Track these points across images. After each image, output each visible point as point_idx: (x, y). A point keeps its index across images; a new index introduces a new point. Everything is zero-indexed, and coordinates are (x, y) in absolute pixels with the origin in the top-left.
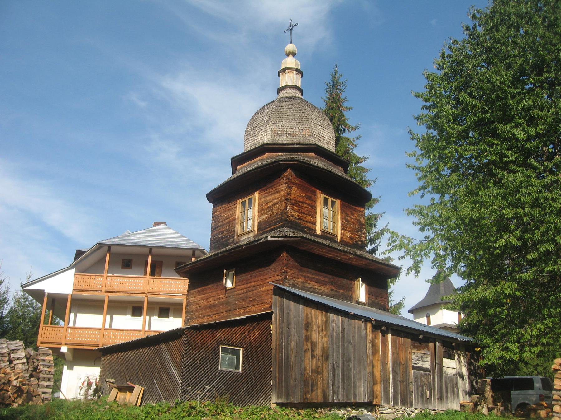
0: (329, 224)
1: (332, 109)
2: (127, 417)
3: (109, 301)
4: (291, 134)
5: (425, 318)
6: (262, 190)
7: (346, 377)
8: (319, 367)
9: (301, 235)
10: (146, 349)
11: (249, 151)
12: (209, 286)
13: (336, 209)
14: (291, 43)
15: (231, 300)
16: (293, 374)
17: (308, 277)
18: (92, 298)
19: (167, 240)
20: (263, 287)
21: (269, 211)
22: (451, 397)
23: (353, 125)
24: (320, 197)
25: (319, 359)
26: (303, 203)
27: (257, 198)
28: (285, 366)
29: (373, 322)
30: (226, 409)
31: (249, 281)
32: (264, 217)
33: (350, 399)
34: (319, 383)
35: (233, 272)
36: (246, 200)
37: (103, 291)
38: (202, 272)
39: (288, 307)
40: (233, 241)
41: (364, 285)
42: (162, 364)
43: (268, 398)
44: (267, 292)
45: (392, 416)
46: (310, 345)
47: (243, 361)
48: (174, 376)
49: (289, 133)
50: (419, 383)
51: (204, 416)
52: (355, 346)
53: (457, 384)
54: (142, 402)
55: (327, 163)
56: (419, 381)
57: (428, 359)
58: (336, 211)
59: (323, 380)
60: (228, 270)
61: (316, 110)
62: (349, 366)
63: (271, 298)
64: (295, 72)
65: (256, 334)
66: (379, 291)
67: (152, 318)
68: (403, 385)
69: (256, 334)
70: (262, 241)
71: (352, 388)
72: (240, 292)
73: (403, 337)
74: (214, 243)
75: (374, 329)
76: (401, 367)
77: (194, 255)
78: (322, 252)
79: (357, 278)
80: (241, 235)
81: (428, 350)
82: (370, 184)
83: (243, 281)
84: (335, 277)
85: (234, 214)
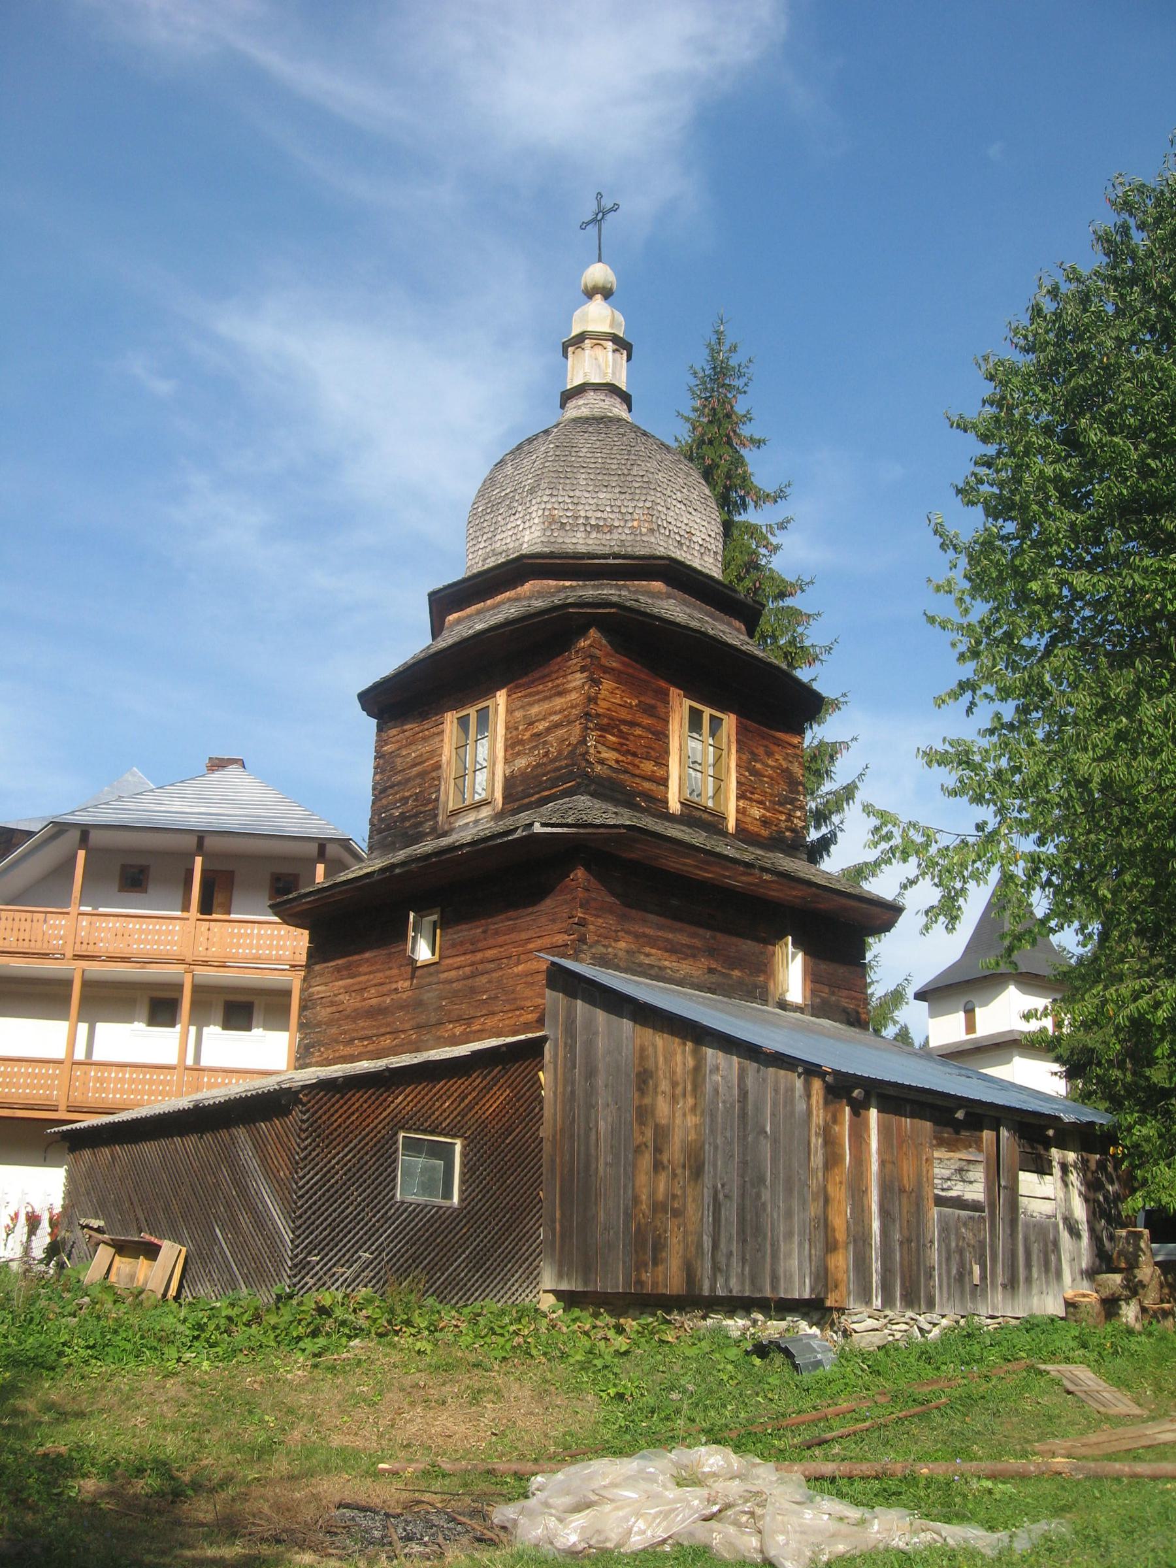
0: (705, 782)
1: (711, 442)
2: (142, 1337)
3: (87, 984)
4: (598, 526)
5: (961, 1016)
6: (517, 687)
7: (752, 1230)
8: (674, 1196)
9: (625, 817)
10: (194, 1138)
11: (480, 574)
12: (367, 955)
13: (725, 740)
14: (600, 260)
15: (428, 996)
16: (602, 1214)
17: (644, 935)
18: (35, 974)
19: (246, 812)
20: (518, 963)
21: (535, 747)
22: (1039, 1278)
23: (770, 489)
24: (680, 706)
25: (675, 1175)
26: (632, 724)
27: (502, 709)
28: (580, 1190)
29: (828, 1078)
30: (417, 1320)
31: (480, 945)
32: (521, 763)
33: (760, 1291)
34: (675, 1240)
35: (435, 917)
36: (472, 712)
37: (69, 954)
38: (349, 917)
39: (589, 1024)
40: (434, 829)
41: (800, 956)
42: (237, 1183)
43: (532, 1277)
44: (529, 979)
45: (877, 1339)
46: (649, 1133)
47: (462, 1174)
48: (272, 1219)
49: (593, 522)
50: (953, 1244)
51: (356, 1336)
52: (775, 1141)
53: (1056, 1244)
54: (181, 1286)
55: (700, 610)
56: (953, 1237)
57: (978, 1174)
58: (724, 746)
59: (685, 1232)
60: (421, 911)
61: (669, 457)
62: (758, 1195)
63: (542, 996)
64: (610, 345)
65: (499, 1097)
66: (841, 970)
67: (205, 1029)
68: (910, 1249)
69: (499, 1097)
70: (516, 836)
71: (768, 1259)
72: (453, 974)
73: (912, 1117)
74: (380, 831)
75: (830, 1097)
76: (905, 1200)
77: (321, 855)
78: (684, 864)
79: (781, 936)
80: (455, 813)
81: (980, 1149)
82: (816, 658)
83: (462, 943)
84: (719, 935)
85: (436, 752)
